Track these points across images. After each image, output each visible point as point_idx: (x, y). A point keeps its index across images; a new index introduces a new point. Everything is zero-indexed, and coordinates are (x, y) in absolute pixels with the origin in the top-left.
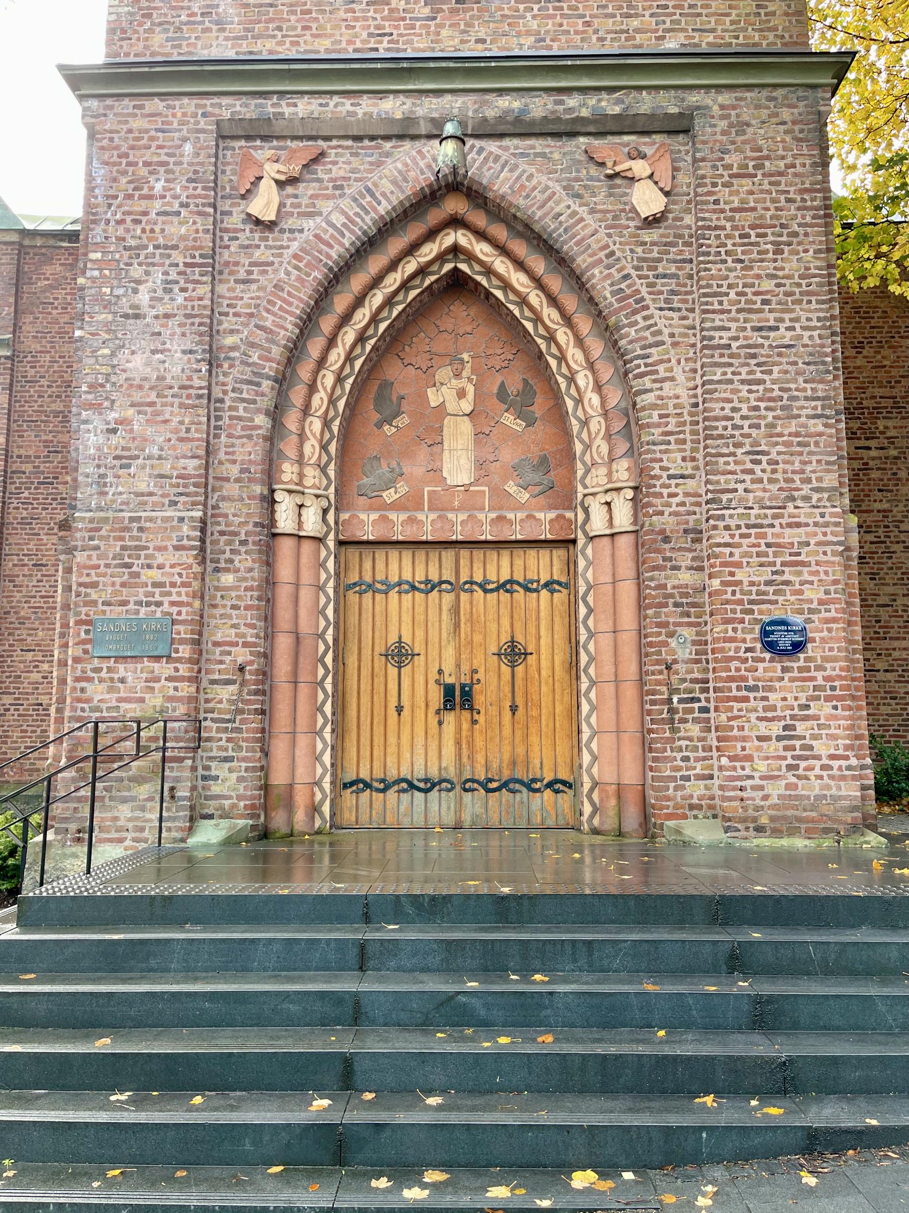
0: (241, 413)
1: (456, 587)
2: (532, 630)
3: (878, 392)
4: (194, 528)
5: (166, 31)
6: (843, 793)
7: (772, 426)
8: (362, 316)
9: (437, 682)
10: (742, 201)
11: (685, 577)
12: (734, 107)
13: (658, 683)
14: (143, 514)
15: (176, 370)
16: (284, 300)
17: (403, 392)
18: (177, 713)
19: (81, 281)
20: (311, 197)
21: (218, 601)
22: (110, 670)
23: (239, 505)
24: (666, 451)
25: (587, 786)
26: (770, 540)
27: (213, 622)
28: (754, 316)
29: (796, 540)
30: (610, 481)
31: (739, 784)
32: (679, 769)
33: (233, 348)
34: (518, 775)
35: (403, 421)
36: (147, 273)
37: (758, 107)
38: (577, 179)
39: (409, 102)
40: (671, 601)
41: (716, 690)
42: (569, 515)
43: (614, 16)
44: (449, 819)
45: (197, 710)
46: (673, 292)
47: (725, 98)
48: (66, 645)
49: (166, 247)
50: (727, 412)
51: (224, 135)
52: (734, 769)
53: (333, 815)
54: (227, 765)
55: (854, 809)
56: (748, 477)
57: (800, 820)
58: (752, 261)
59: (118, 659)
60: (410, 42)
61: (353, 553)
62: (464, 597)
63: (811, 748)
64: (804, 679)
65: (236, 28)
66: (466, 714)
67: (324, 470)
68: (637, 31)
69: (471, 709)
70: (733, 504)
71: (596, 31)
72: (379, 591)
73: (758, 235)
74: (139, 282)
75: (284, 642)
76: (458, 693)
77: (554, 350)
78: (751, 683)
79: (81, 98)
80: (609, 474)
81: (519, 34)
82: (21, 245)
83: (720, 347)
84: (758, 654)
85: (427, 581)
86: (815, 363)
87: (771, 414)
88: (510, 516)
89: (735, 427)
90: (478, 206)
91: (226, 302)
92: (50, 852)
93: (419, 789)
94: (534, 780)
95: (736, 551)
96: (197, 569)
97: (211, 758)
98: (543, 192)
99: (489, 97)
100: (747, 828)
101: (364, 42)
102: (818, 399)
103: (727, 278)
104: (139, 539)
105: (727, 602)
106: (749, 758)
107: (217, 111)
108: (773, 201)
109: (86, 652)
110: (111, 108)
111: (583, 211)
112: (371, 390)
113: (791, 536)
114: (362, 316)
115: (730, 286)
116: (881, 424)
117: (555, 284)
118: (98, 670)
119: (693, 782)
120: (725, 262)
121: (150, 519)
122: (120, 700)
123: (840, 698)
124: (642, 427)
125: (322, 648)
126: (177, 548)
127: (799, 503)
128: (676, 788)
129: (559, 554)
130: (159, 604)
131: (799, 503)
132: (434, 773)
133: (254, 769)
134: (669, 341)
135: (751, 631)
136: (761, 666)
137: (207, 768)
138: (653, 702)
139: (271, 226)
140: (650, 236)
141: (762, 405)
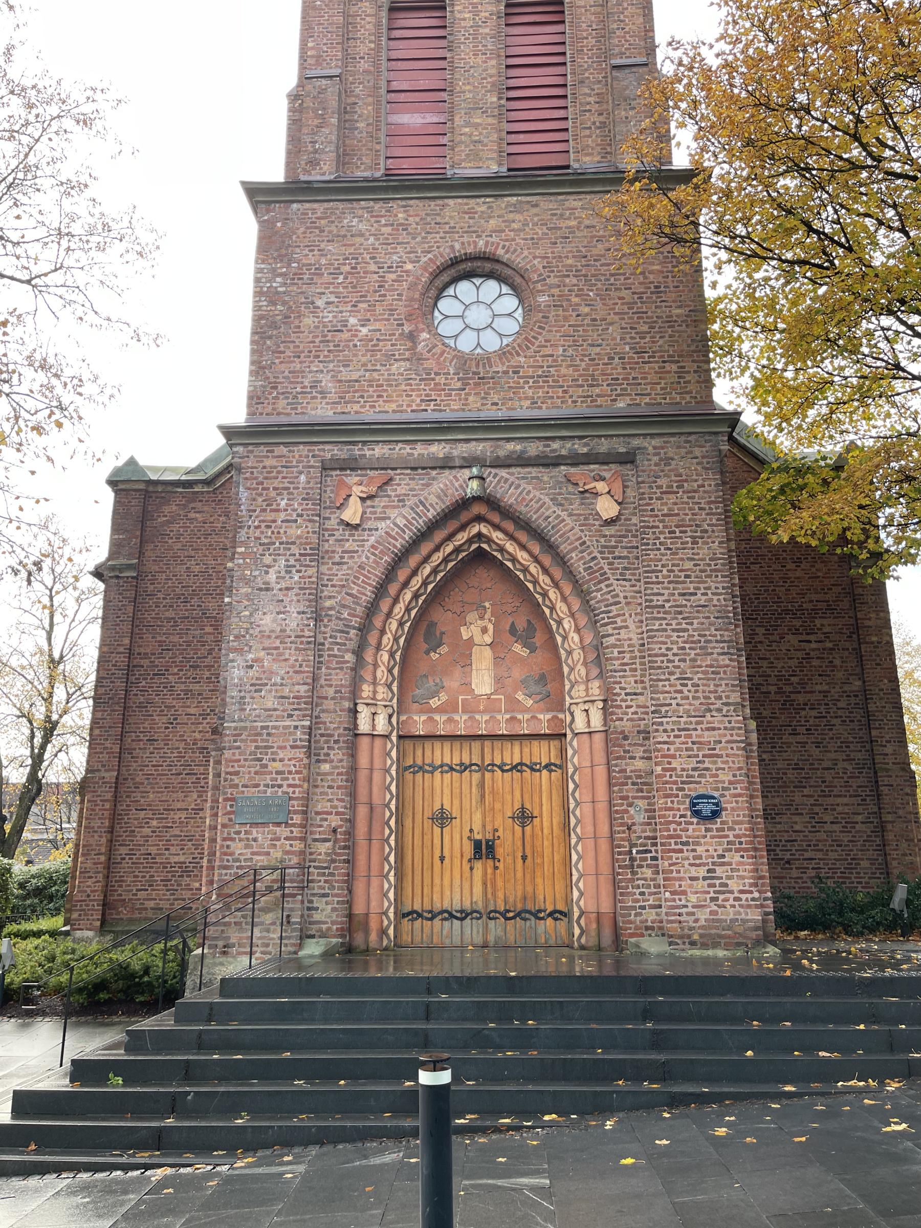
0: (336, 652)
1: (482, 768)
2: (536, 799)
3: (814, 597)
4: (304, 733)
5: (287, 398)
6: (749, 917)
8: (416, 582)
9: (469, 838)
10: (669, 510)
11: (639, 764)
12: (663, 448)
13: (623, 839)
14: (271, 724)
15: (293, 625)
16: (365, 576)
17: (443, 630)
18: (292, 863)
20: (384, 507)
23: (333, 715)
24: (624, 677)
25: (576, 915)
26: (694, 739)
27: (315, 798)
28: (680, 586)
29: (712, 739)
30: (587, 695)
31: (678, 911)
32: (637, 901)
33: (331, 609)
34: (528, 907)
35: (444, 649)
36: (275, 561)
37: (679, 447)
38: (560, 494)
39: (448, 446)
40: (630, 781)
41: (662, 844)
42: (561, 716)
43: (582, 386)
44: (479, 940)
45: (304, 860)
46: (625, 568)
47: (656, 442)
48: (216, 815)
49: (287, 543)
50: (663, 650)
51: (326, 467)
52: (674, 900)
53: (395, 937)
54: (324, 899)
55: (756, 929)
56: (679, 696)
57: (720, 936)
58: (677, 549)
59: (254, 825)
60: (449, 405)
61: (409, 744)
62: (488, 775)
63: (726, 885)
65: (333, 397)
67: (389, 687)
68: (598, 396)
69: (494, 858)
70: (669, 714)
71: (571, 397)
72: (428, 772)
73: (681, 532)
74: (269, 567)
76: (484, 847)
77: (548, 602)
78: (684, 839)
80: (587, 690)
81: (520, 399)
82: (146, 491)
84: (688, 819)
85: (461, 764)
86: (722, 618)
87: (693, 652)
88: (520, 717)
89: (669, 661)
91: (326, 578)
92: (206, 961)
93: (457, 918)
94: (540, 911)
96: (306, 761)
97: (314, 895)
98: (537, 502)
99: (501, 443)
100: (684, 943)
101: (417, 405)
102: (725, 642)
103: (661, 560)
104: (267, 741)
105: (667, 782)
106: (684, 893)
107: (322, 454)
108: (690, 509)
109: (230, 820)
110: (252, 452)
111: (564, 514)
112: (423, 630)
113: (708, 736)
114: (416, 582)
115: (663, 566)
116: (818, 622)
117: (547, 560)
118: (239, 833)
119: (647, 910)
120: (659, 549)
122: (253, 854)
124: (607, 659)
125: (388, 814)
126: (292, 747)
127: (714, 713)
129: (555, 744)
130: (280, 786)
131: (714, 713)
132: (467, 905)
133: (343, 902)
134: (623, 601)
135: (684, 803)
136: (691, 827)
137: (311, 902)
138: (620, 853)
139: (356, 527)
140: (607, 531)
141: (687, 646)
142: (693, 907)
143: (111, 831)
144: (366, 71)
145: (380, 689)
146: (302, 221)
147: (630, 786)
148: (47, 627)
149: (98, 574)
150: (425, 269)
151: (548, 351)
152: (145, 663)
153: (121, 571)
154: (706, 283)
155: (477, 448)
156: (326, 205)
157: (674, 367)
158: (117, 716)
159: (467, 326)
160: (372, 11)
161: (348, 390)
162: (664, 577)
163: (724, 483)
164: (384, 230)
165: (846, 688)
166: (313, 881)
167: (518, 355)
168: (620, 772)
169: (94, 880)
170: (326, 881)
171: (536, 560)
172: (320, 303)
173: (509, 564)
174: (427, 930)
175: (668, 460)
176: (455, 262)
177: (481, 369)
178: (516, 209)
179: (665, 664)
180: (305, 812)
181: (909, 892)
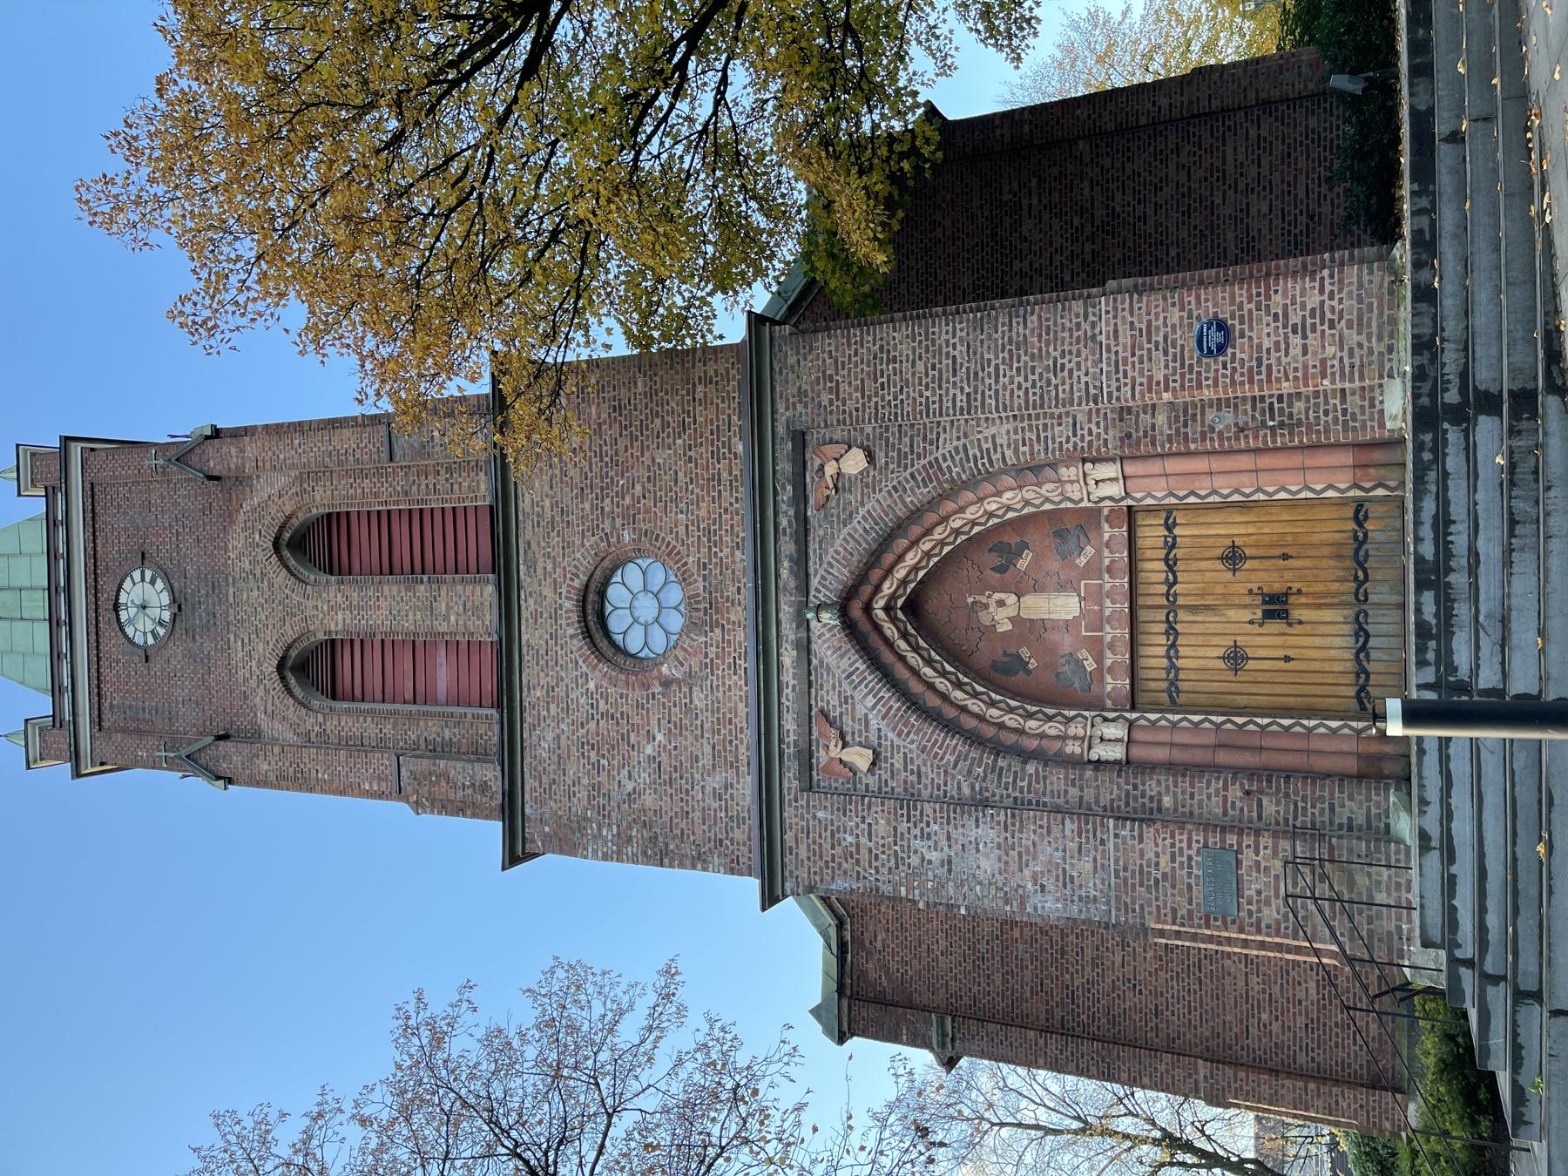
0: (1025, 784)
1: (1172, 607)
4: (1124, 826)
7: (1033, 357)
9: (1261, 625)
11: (1161, 419)
15: (992, 834)
19: (921, 906)
21: (1186, 810)
22: (1250, 903)
25: (1359, 493)
26: (1128, 354)
31: (1347, 369)
32: (1336, 419)
33: (973, 788)
35: (1025, 652)
36: (916, 852)
37: (787, 382)
42: (1105, 512)
47: (781, 407)
49: (895, 836)
51: (809, 787)
52: (1333, 374)
54: (1337, 809)
56: (1076, 374)
59: (1239, 893)
61: (1142, 698)
62: (1181, 601)
63: (1313, 310)
64: (1251, 319)
65: (731, 774)
66: (1292, 599)
67: (1070, 720)
69: (1286, 595)
72: (1177, 675)
74: (923, 859)
75: (1223, 757)
78: (1254, 363)
79: (785, 896)
80: (1072, 482)
83: (969, 402)
85: (1167, 633)
88: (1107, 562)
89: (1034, 386)
90: (856, 592)
93: (1366, 642)
94: (1356, 538)
95: (1138, 380)
96: (1159, 825)
97: (1331, 823)
104: (1133, 872)
105: (1182, 386)
106: (1323, 362)
109: (1234, 922)
110: (791, 872)
113: (1125, 337)
114: (942, 684)
117: (916, 530)
118: (1250, 913)
119: (1348, 406)
121: (1117, 861)
122: (1277, 896)
123: (1268, 289)
125: (1229, 726)
126: (1141, 841)
127: (1097, 331)
128: (1354, 420)
129: (1141, 520)
130: (1190, 858)
132: (1348, 629)
134: (963, 440)
135: (1208, 365)
136: (1238, 355)
137: (1341, 826)
139: (876, 754)
140: (881, 458)
142: (1342, 350)
143: (1275, 1072)
144: (395, 725)
145: (1072, 731)
146: (543, 804)
147: (1189, 430)
148: (1040, 1133)
149: (950, 1063)
150: (595, 668)
151: (682, 530)
152: (1058, 1013)
153: (944, 1035)
154: (604, 355)
155: (787, 611)
156: (527, 776)
157: (700, 388)
158: (1126, 1053)
159: (657, 620)
160: (335, 718)
161: (722, 757)
162: (934, 394)
163: (828, 329)
164: (553, 713)
165: (1087, 159)
166: (1313, 823)
167: (686, 564)
168: (1170, 442)
169: (1340, 1099)
170: (1313, 806)
171: (915, 543)
172: (630, 787)
173: (921, 574)
174: (1380, 679)
175: (801, 393)
176: (587, 634)
177: (701, 606)
178: (532, 566)
179: (1037, 390)
180: (1223, 830)
181: (1342, 72)
